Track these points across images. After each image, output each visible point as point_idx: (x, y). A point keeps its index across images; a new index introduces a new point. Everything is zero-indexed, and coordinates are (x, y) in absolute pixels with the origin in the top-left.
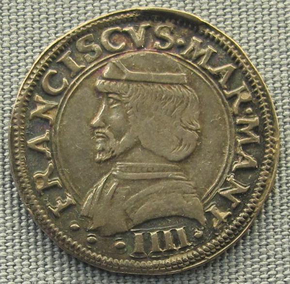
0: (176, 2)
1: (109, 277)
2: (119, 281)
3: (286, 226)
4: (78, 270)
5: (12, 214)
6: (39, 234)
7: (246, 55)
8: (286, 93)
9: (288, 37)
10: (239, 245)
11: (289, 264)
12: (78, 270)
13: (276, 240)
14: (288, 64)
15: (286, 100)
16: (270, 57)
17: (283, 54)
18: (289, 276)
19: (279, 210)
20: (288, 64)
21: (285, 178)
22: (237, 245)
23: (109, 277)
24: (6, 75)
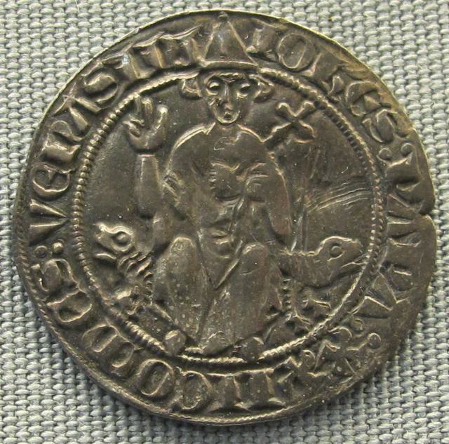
2: (269, 435)
3: (442, 135)
13: (438, 151)
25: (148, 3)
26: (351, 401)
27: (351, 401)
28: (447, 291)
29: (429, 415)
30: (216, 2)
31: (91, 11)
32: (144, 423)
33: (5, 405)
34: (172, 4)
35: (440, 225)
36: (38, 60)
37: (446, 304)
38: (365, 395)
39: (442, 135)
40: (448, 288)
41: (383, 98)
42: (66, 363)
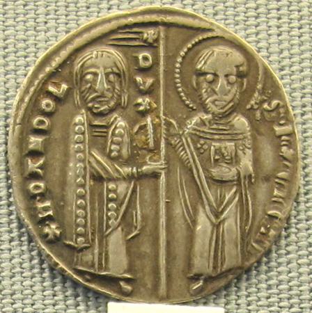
0: (117, 2)
1: (97, 298)
3: (307, 55)
4: (76, 296)
5: (32, 268)
6: (46, 270)
7: (231, 32)
8: (306, 296)
9: (309, 235)
10: (231, 286)
11: (311, 98)
12: (76, 296)
13: (280, 273)
14: (309, 265)
15: (307, 46)
16: (278, 50)
17: (303, 258)
18: (310, 131)
19: (286, 295)
20: (309, 265)
21: (306, 9)
22: (227, 287)
23: (97, 298)
24: (48, 299)
25: (224, 3)
26: (223, 300)
27: (224, 293)
28: (311, 270)
29: (291, 292)
30: (220, 2)
31: (7, 68)
32: (89, 303)
33: (4, 307)
34: (224, 3)
35: (305, 185)
36: (232, 9)
37: (308, 244)
38: (236, 289)
39: (307, 72)
40: (311, 257)
41: (154, 182)
42: (44, 269)
